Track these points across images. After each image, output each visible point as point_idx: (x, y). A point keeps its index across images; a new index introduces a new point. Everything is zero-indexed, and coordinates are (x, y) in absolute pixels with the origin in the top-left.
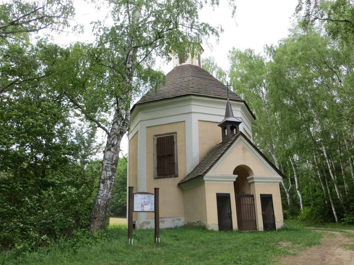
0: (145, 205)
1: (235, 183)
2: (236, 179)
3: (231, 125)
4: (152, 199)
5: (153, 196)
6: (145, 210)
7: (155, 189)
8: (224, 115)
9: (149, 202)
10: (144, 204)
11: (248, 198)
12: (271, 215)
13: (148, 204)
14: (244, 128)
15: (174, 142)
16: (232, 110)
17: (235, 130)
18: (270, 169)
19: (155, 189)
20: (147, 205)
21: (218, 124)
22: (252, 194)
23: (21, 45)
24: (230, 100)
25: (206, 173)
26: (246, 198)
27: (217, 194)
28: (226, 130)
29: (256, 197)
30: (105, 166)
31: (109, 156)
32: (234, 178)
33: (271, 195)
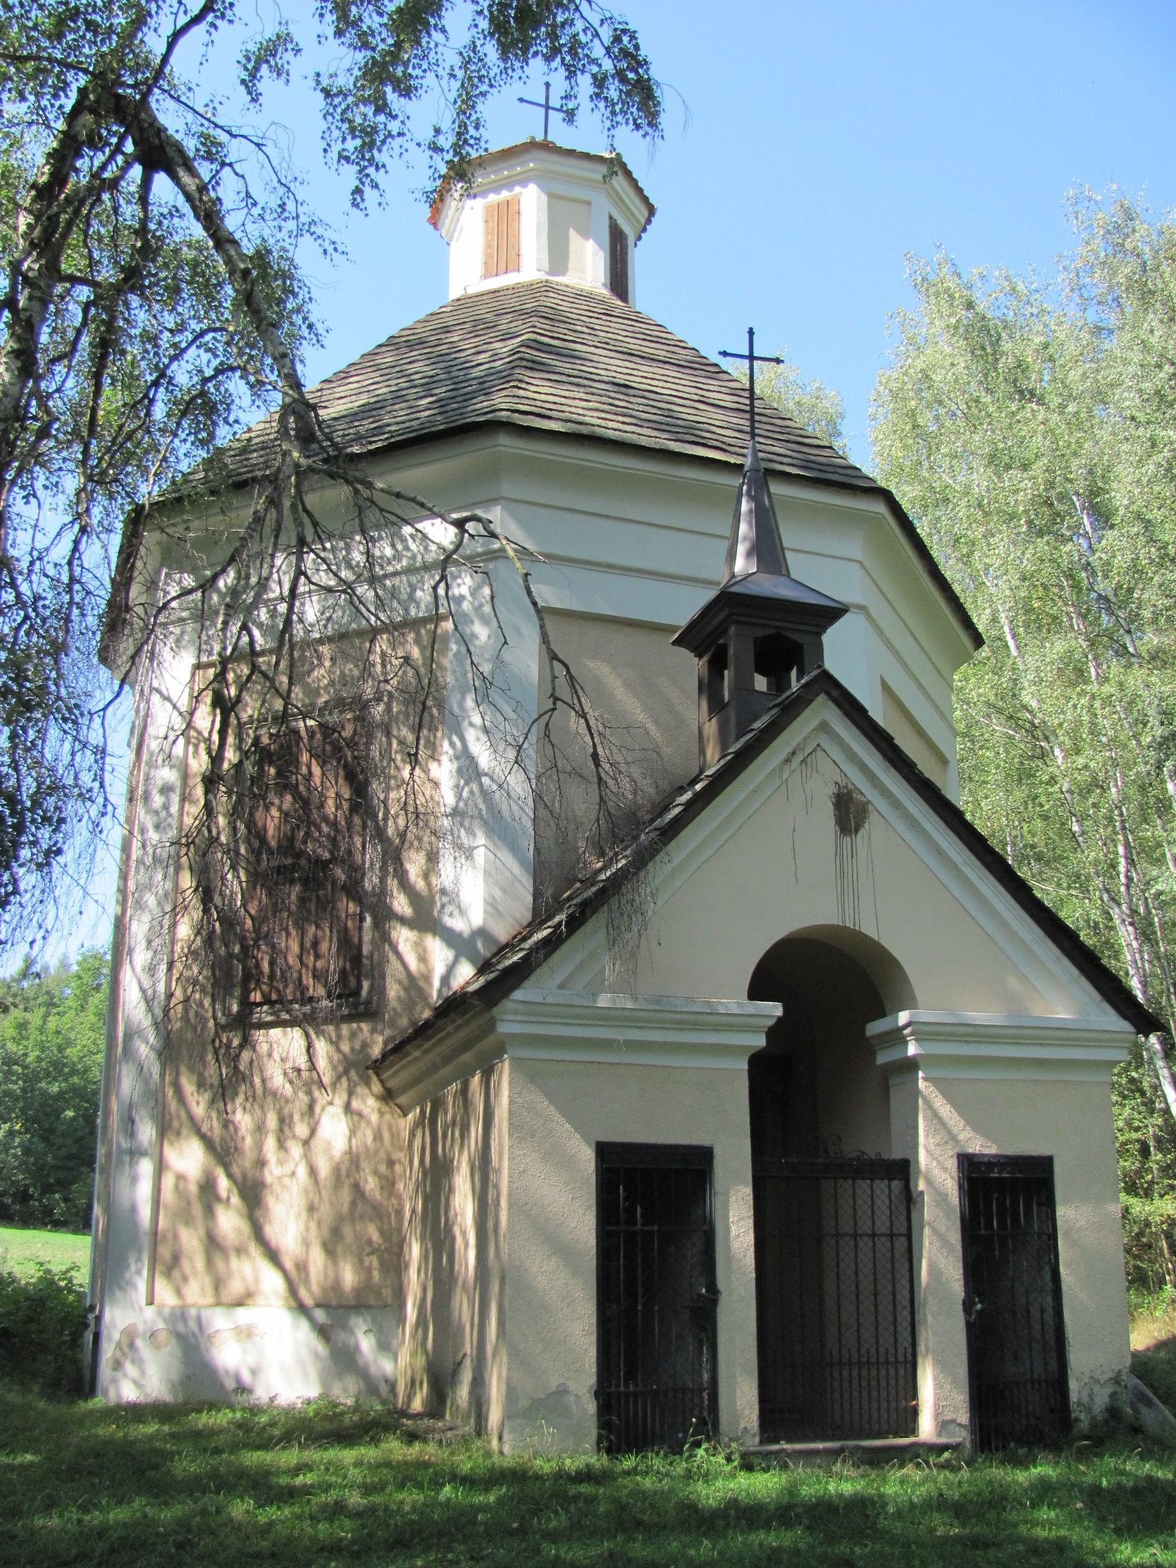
1: (757, 1062)
3: (761, 633)
14: (884, 684)
18: (993, 914)
22: (896, 1154)
23: (104, 153)
25: (517, 985)
32: (754, 1029)
33: (1045, 1164)
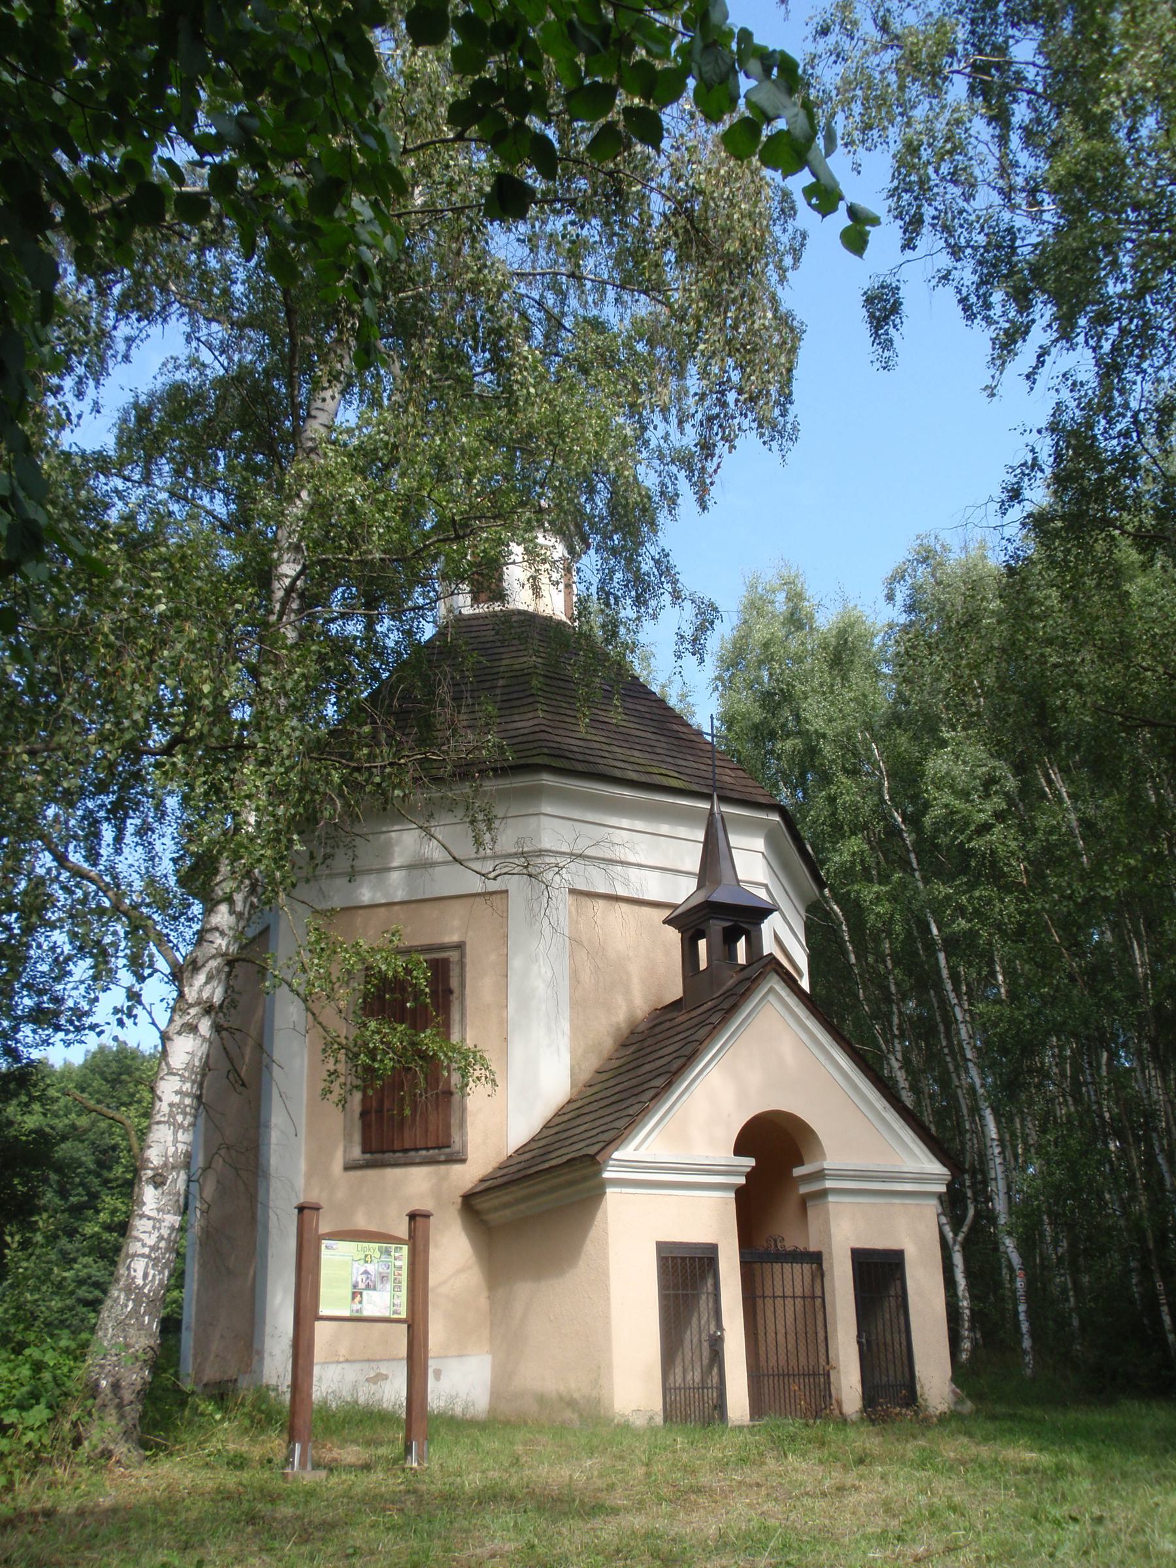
0: (368, 1287)
2: (748, 1176)
4: (398, 1263)
5: (405, 1248)
6: (368, 1312)
7: (413, 1216)
8: (697, 870)
9: (383, 1278)
10: (362, 1285)
11: (797, 1267)
12: (897, 1346)
13: (379, 1286)
15: (451, 992)
16: (729, 848)
17: (741, 945)
19: (413, 1216)
20: (375, 1289)
21: (666, 913)
22: (813, 1248)
24: (724, 799)
26: (787, 1266)
27: (661, 1247)
28: (702, 944)
29: (832, 1264)
30: (171, 1105)
31: (186, 1058)
